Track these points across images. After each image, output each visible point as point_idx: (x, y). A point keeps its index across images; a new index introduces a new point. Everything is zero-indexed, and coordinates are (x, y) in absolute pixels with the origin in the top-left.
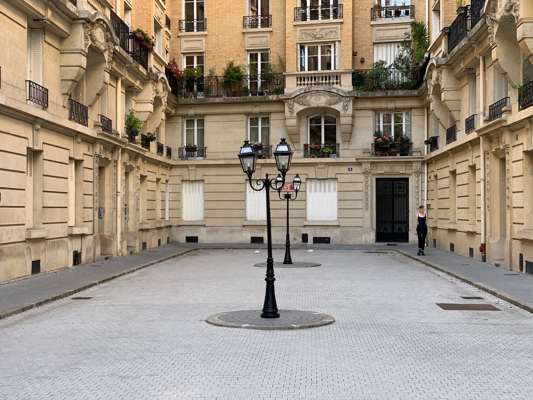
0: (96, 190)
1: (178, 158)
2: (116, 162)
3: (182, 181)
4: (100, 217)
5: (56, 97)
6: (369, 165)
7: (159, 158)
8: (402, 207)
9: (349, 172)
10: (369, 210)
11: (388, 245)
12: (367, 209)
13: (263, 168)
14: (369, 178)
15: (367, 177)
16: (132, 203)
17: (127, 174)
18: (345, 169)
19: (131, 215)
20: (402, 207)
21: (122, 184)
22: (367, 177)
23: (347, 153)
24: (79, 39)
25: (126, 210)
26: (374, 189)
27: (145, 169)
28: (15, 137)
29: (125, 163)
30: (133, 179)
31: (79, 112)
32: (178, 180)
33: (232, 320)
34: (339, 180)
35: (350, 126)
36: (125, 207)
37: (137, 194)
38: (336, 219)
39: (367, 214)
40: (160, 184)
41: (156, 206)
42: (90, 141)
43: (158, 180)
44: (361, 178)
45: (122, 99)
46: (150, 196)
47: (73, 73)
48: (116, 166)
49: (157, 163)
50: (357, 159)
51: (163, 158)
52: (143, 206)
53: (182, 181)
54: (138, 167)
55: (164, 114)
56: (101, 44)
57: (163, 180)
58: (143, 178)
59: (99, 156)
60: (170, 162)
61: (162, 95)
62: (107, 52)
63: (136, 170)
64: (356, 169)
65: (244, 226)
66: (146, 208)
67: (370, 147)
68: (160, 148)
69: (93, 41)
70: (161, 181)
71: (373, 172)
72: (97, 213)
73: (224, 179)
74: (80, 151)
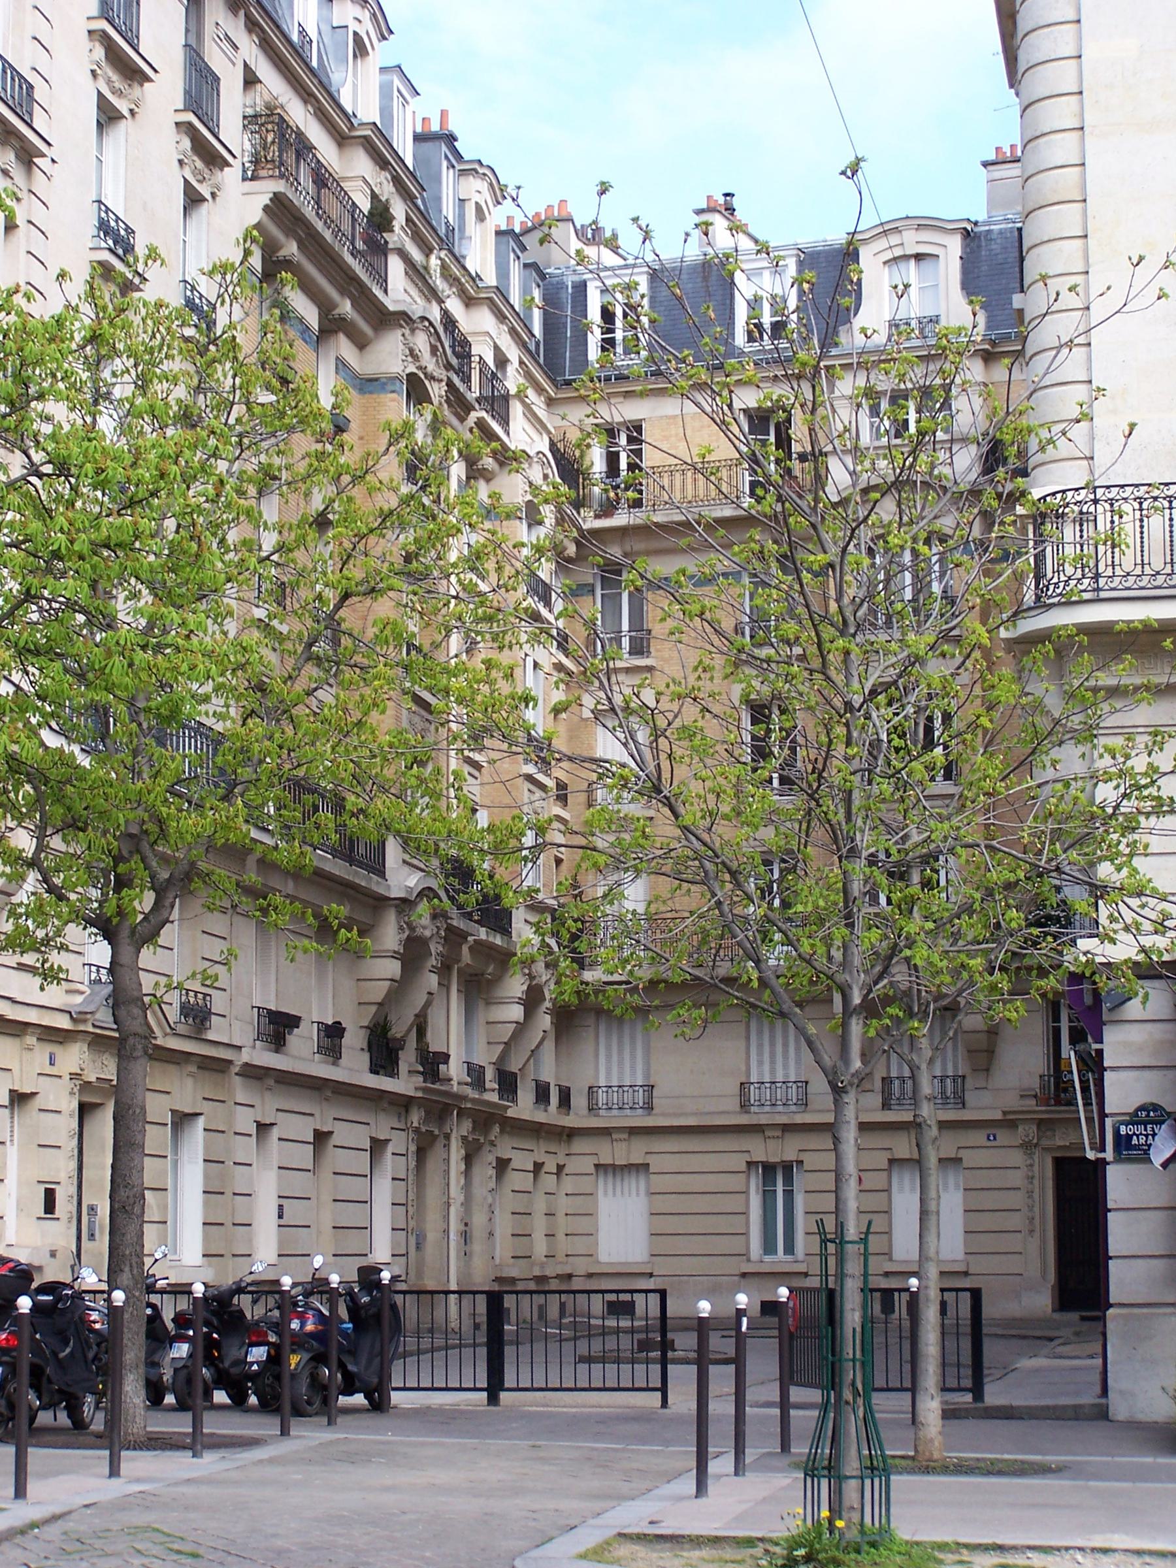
0: (411, 1196)
1: (586, 1112)
2: (447, 1137)
3: (597, 1166)
4: (419, 1247)
5: (354, 1040)
6: (1035, 1128)
7: (540, 1117)
8: (710, 1224)
9: (989, 1144)
10: (1037, 1234)
11: (1083, 1319)
12: (1031, 1231)
13: (787, 1135)
14: (1036, 1157)
15: (1031, 1155)
16: (479, 1219)
17: (468, 1159)
18: (979, 1137)
19: (477, 1247)
20: (710, 1224)
21: (458, 1181)
22: (1031, 1155)
23: (986, 1098)
24: (390, 935)
25: (466, 1237)
26: (1050, 1184)
27: (505, 1148)
28: (892, 1494)
29: (464, 1138)
30: (484, 1171)
31: (383, 1052)
32: (588, 1165)
33: (229, 970)
34: (965, 1164)
35: (983, 1037)
36: (463, 1228)
37: (490, 1200)
38: (960, 1256)
39: (1033, 1244)
40: (543, 1176)
41: (206, 1204)
42: (402, 1104)
43: (538, 1167)
44: (1017, 1158)
45: (458, 1035)
46: (519, 1203)
47: (378, 991)
48: (447, 1146)
49: (536, 1130)
50: (1005, 1113)
51: (551, 1115)
52: (504, 1225)
53: (597, 1166)
54: (493, 1144)
55: (548, 1017)
56: (424, 928)
57: (551, 1167)
58: (502, 1165)
59: (417, 1130)
60: (569, 1121)
61: (544, 979)
62: (435, 939)
63: (487, 1147)
64: (1003, 1137)
65: (744, 1275)
66: (510, 1232)
67: (1035, 1083)
68: (542, 1094)
69: (412, 928)
70: (546, 1168)
71: (1045, 1143)
72: (413, 1241)
73: (695, 1163)
74: (383, 1126)
